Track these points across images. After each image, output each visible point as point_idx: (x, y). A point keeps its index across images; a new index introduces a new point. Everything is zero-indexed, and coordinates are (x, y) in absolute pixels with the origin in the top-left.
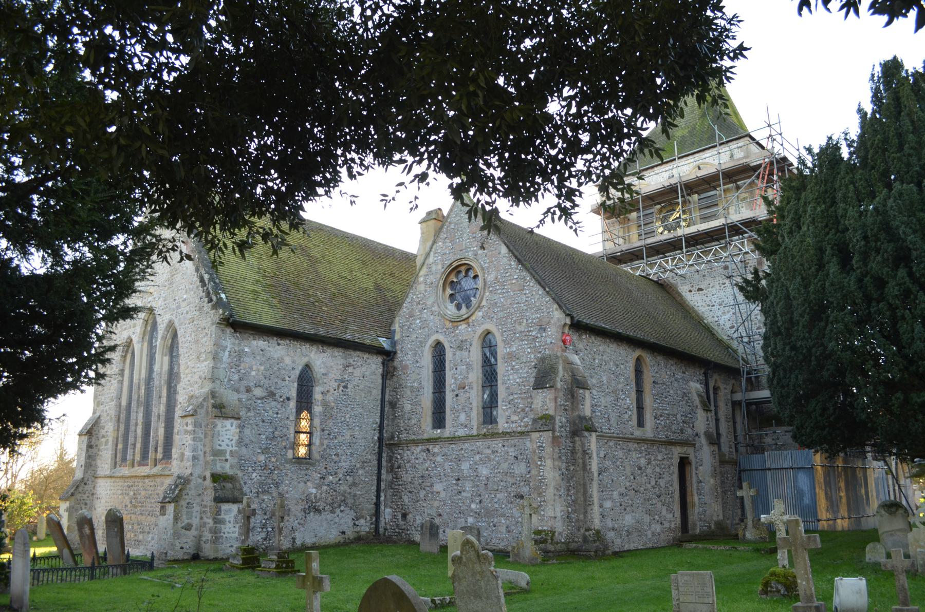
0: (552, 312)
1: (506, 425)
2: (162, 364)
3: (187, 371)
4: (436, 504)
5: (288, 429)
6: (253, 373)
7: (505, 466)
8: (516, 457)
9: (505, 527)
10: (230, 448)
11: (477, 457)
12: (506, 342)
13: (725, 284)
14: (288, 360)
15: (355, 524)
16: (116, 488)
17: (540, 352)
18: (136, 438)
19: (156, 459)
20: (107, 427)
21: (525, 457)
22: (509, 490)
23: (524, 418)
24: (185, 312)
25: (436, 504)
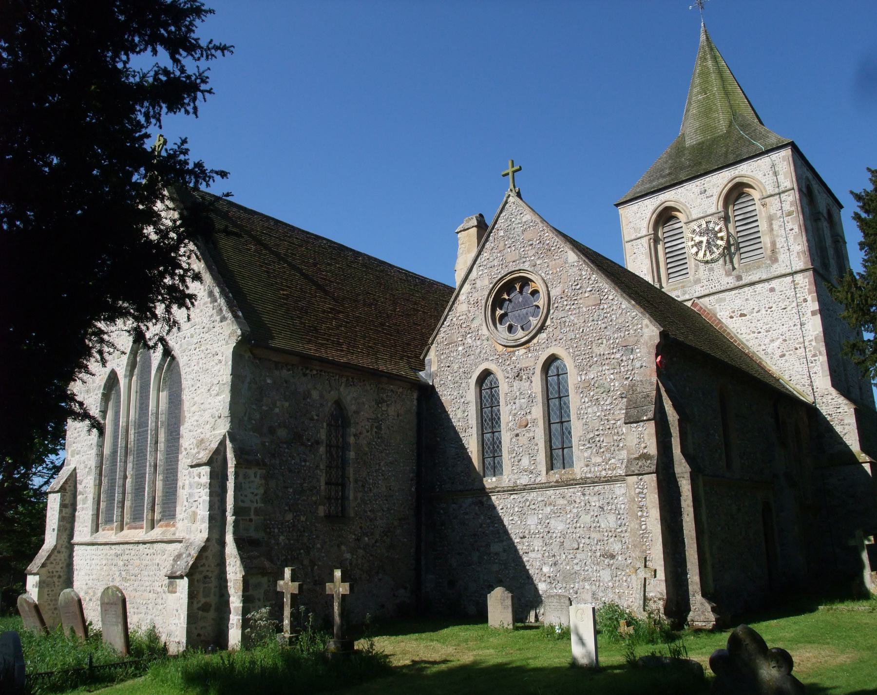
0: (641, 328)
1: (586, 469)
2: (159, 400)
3: (193, 409)
4: (495, 568)
5: (318, 481)
6: (277, 410)
7: (586, 519)
8: (602, 508)
9: (590, 595)
10: (255, 505)
11: (548, 509)
12: (581, 369)
13: (771, 308)
14: (315, 394)
15: (394, 595)
16: (99, 557)
17: (627, 379)
18: (124, 493)
19: (153, 520)
20: (85, 482)
21: (614, 507)
22: (594, 548)
23: (610, 460)
24: (189, 335)
25: (495, 568)
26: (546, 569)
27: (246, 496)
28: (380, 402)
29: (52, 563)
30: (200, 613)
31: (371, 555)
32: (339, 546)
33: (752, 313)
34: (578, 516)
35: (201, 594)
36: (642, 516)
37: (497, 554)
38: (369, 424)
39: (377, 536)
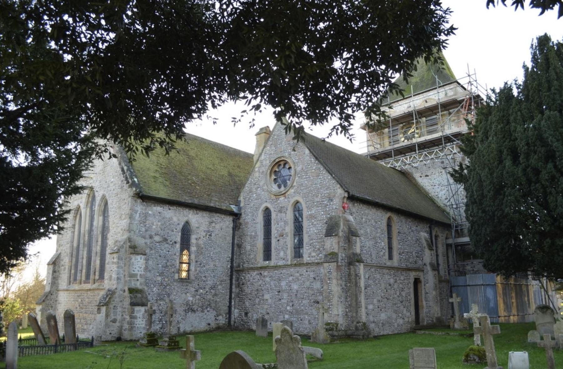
0: (337, 189)
1: (308, 259)
2: (98, 221)
3: (114, 226)
4: (266, 307)
7: (308, 284)
8: (315, 278)
10: (140, 273)
11: (291, 278)
14: (175, 219)
15: (216, 319)
17: (329, 214)
18: (82, 266)
22: (310, 298)
24: (112, 189)
25: (266, 307)
26: (288, 308)
27: (135, 268)
28: (211, 223)
29: (48, 300)
30: (111, 323)
31: (204, 299)
32: (186, 294)
33: (432, 175)
34: (304, 282)
35: (112, 314)
36: (330, 283)
37: (267, 300)
38: (205, 233)
39: (207, 289)
